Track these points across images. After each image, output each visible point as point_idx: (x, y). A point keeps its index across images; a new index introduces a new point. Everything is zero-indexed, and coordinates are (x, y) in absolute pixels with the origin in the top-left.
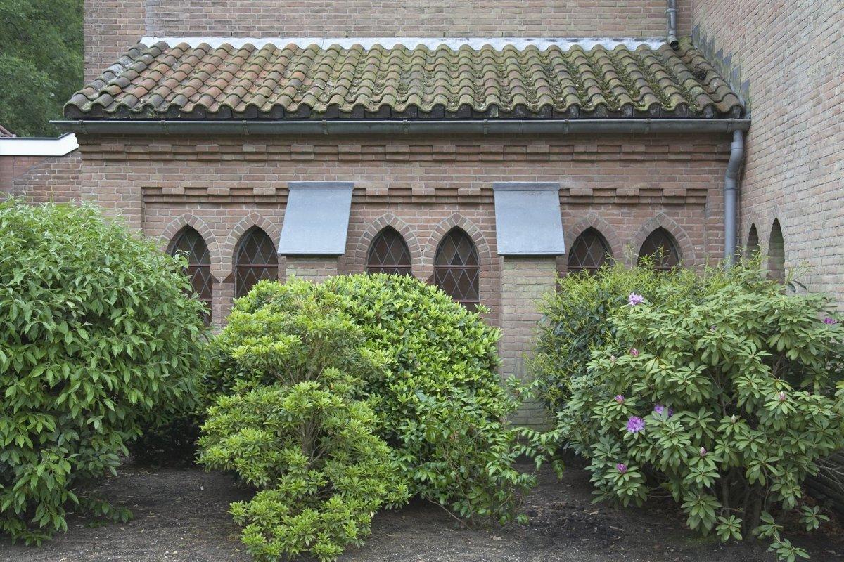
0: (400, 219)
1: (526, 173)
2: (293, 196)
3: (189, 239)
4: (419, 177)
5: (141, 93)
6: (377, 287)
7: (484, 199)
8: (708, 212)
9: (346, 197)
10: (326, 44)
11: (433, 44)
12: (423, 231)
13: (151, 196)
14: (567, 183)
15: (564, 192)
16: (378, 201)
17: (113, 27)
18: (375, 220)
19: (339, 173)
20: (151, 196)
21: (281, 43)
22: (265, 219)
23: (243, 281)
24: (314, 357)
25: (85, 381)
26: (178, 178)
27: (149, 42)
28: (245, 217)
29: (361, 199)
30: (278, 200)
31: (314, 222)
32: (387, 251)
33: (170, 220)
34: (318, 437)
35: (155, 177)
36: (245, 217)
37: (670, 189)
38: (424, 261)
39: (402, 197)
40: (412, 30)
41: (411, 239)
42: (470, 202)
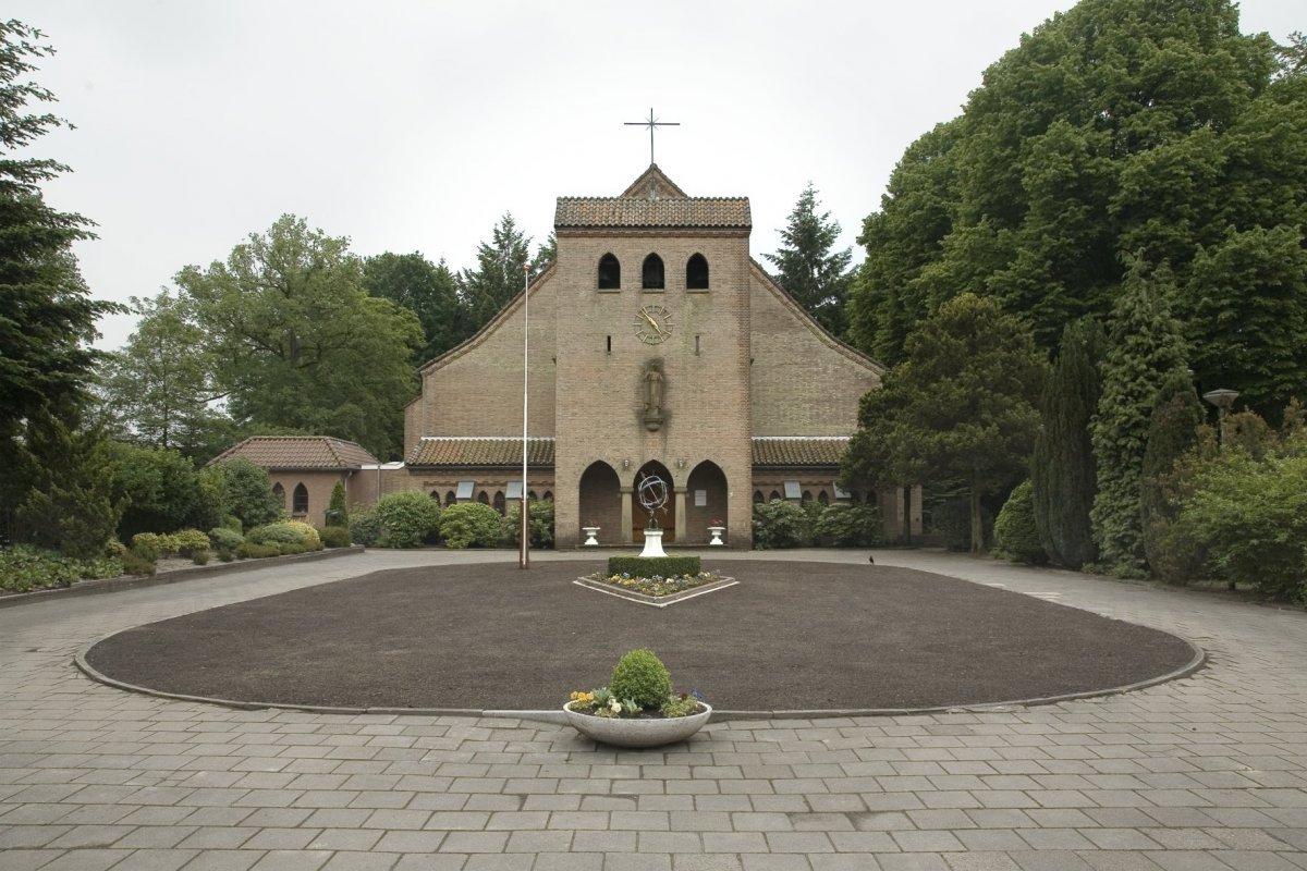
0: (486, 489)
1: (465, 478)
2: (509, 484)
3: (435, 495)
5: (426, 458)
6: (475, 505)
10: (471, 439)
11: (500, 439)
12: (491, 492)
13: (426, 484)
16: (479, 485)
17: (412, 434)
18: (480, 489)
19: (469, 478)
20: (426, 484)
21: (459, 439)
22: (453, 489)
23: (447, 504)
24: (460, 516)
25: (421, 520)
27: (423, 439)
28: (448, 488)
29: (476, 485)
31: (464, 491)
32: (483, 497)
33: (431, 489)
34: (458, 529)
35: (427, 480)
36: (448, 488)
37: (491, 482)
38: (491, 500)
41: (489, 494)
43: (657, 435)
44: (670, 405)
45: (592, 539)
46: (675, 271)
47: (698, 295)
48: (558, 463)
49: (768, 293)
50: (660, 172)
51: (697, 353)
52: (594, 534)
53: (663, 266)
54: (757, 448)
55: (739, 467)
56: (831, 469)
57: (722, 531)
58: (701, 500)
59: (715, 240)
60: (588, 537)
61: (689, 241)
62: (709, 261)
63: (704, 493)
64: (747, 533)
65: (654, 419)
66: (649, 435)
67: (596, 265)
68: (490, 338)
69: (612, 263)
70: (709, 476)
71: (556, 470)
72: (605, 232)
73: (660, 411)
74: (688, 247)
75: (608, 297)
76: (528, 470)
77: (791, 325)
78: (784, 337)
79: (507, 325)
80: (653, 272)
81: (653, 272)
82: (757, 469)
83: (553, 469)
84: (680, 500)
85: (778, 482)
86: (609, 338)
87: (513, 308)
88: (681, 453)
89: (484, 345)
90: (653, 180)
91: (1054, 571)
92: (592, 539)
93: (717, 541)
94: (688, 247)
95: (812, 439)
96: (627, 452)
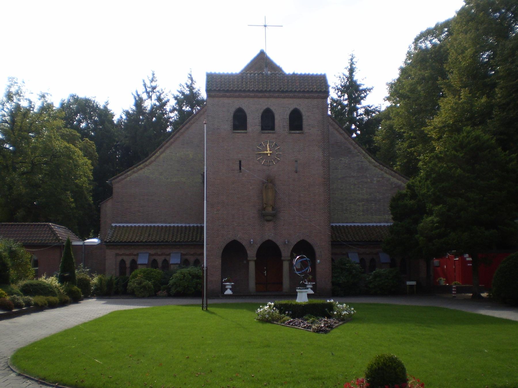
0: (156, 258)
4: (159, 251)
7: (169, 255)
8: (354, 239)
9: (148, 254)
13: (117, 255)
14: (182, 252)
15: (181, 253)
16: (153, 255)
26: (122, 252)
27: (113, 225)
29: (150, 255)
30: (137, 255)
35: (118, 251)
36: (132, 257)
39: (156, 254)
40: (161, 222)
42: (135, 255)
43: (271, 223)
49: (336, 132)
57: (313, 285)
60: (226, 289)
61: (291, 101)
70: (303, 248)
75: (240, 135)
79: (168, 151)
80: (268, 120)
82: (335, 244)
86: (240, 162)
88: (285, 236)
96: (252, 237)
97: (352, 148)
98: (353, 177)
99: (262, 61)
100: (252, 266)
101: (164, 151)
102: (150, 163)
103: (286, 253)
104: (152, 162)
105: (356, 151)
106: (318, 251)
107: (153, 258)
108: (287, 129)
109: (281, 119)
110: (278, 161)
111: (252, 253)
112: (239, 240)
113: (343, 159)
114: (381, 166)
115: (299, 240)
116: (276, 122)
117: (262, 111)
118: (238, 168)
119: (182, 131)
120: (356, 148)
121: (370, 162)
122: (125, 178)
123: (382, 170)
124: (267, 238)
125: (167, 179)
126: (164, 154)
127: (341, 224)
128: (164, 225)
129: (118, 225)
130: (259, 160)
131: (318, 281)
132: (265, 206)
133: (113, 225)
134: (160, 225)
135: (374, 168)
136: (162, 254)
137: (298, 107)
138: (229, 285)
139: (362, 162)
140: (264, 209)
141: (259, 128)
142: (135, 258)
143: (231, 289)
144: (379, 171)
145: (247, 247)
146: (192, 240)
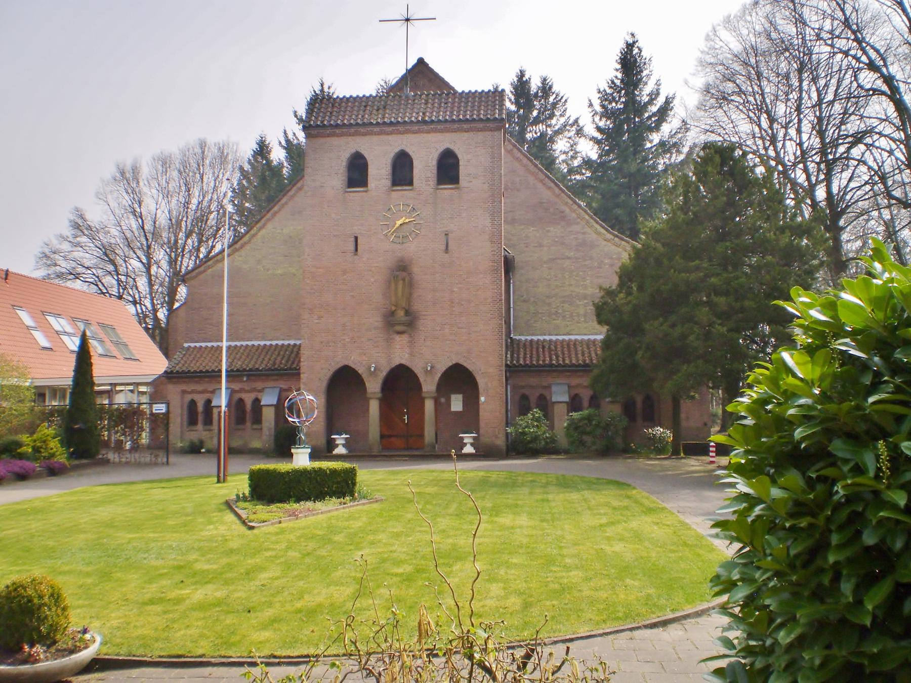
7: (549, 387)
22: (259, 396)
27: (186, 345)
28: (206, 396)
35: (184, 387)
36: (206, 396)
40: (257, 339)
43: (405, 338)
44: (417, 306)
45: (340, 447)
46: (424, 167)
47: (447, 191)
48: (304, 365)
49: (540, 185)
50: (426, 65)
51: (447, 250)
52: (471, 441)
53: (412, 163)
54: (588, 348)
55: (491, 370)
56: (585, 368)
57: (474, 438)
58: (457, 404)
59: (466, 134)
60: (337, 446)
61: (439, 136)
62: (460, 156)
63: (460, 397)
64: (501, 442)
65: (401, 319)
66: (398, 338)
67: (344, 164)
68: (254, 240)
69: (451, 161)
70: (459, 378)
71: (302, 376)
72: (352, 130)
73: (407, 313)
74: (438, 142)
75: (357, 194)
76: (227, 376)
77: (563, 217)
78: (555, 231)
79: (270, 226)
80: (402, 170)
81: (402, 170)
82: (512, 371)
83: (299, 374)
84: (429, 405)
85: (545, 384)
86: (356, 238)
87: (276, 209)
88: (428, 357)
89: (248, 247)
90: (421, 73)
91: (83, 472)
92: (340, 447)
93: (468, 449)
94: (438, 142)
95: (586, 338)
96: (373, 359)
97: (567, 210)
98: (569, 258)
99: (421, 73)
100: (374, 407)
101: (264, 226)
102: (242, 247)
103: (429, 386)
104: (246, 243)
105: (574, 215)
106: (481, 382)
107: (237, 396)
108: (433, 182)
109: (424, 167)
110: (417, 235)
111: (374, 386)
112: (353, 366)
113: (552, 229)
114: (616, 239)
115: (451, 364)
116: (416, 171)
117: (392, 155)
118: (353, 248)
119: (291, 193)
120: (574, 211)
121: (599, 234)
122: (205, 271)
123: (618, 246)
124: (396, 361)
125: (268, 270)
126: (263, 232)
127: (547, 338)
128: (262, 343)
129: (192, 345)
130: (386, 235)
131: (481, 431)
132: (393, 308)
133: (186, 345)
134: (256, 343)
135: (605, 243)
136: (253, 390)
137: (452, 147)
138: (340, 439)
139: (584, 233)
140: (393, 313)
141: (388, 183)
142: (544, 392)
143: (344, 445)
144: (613, 247)
145: (365, 376)
146: (285, 368)
